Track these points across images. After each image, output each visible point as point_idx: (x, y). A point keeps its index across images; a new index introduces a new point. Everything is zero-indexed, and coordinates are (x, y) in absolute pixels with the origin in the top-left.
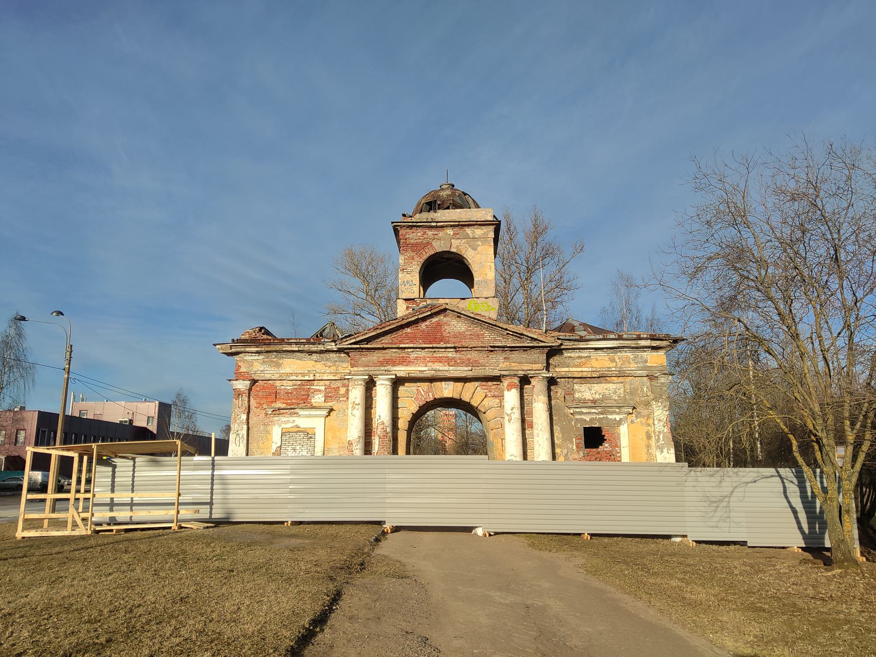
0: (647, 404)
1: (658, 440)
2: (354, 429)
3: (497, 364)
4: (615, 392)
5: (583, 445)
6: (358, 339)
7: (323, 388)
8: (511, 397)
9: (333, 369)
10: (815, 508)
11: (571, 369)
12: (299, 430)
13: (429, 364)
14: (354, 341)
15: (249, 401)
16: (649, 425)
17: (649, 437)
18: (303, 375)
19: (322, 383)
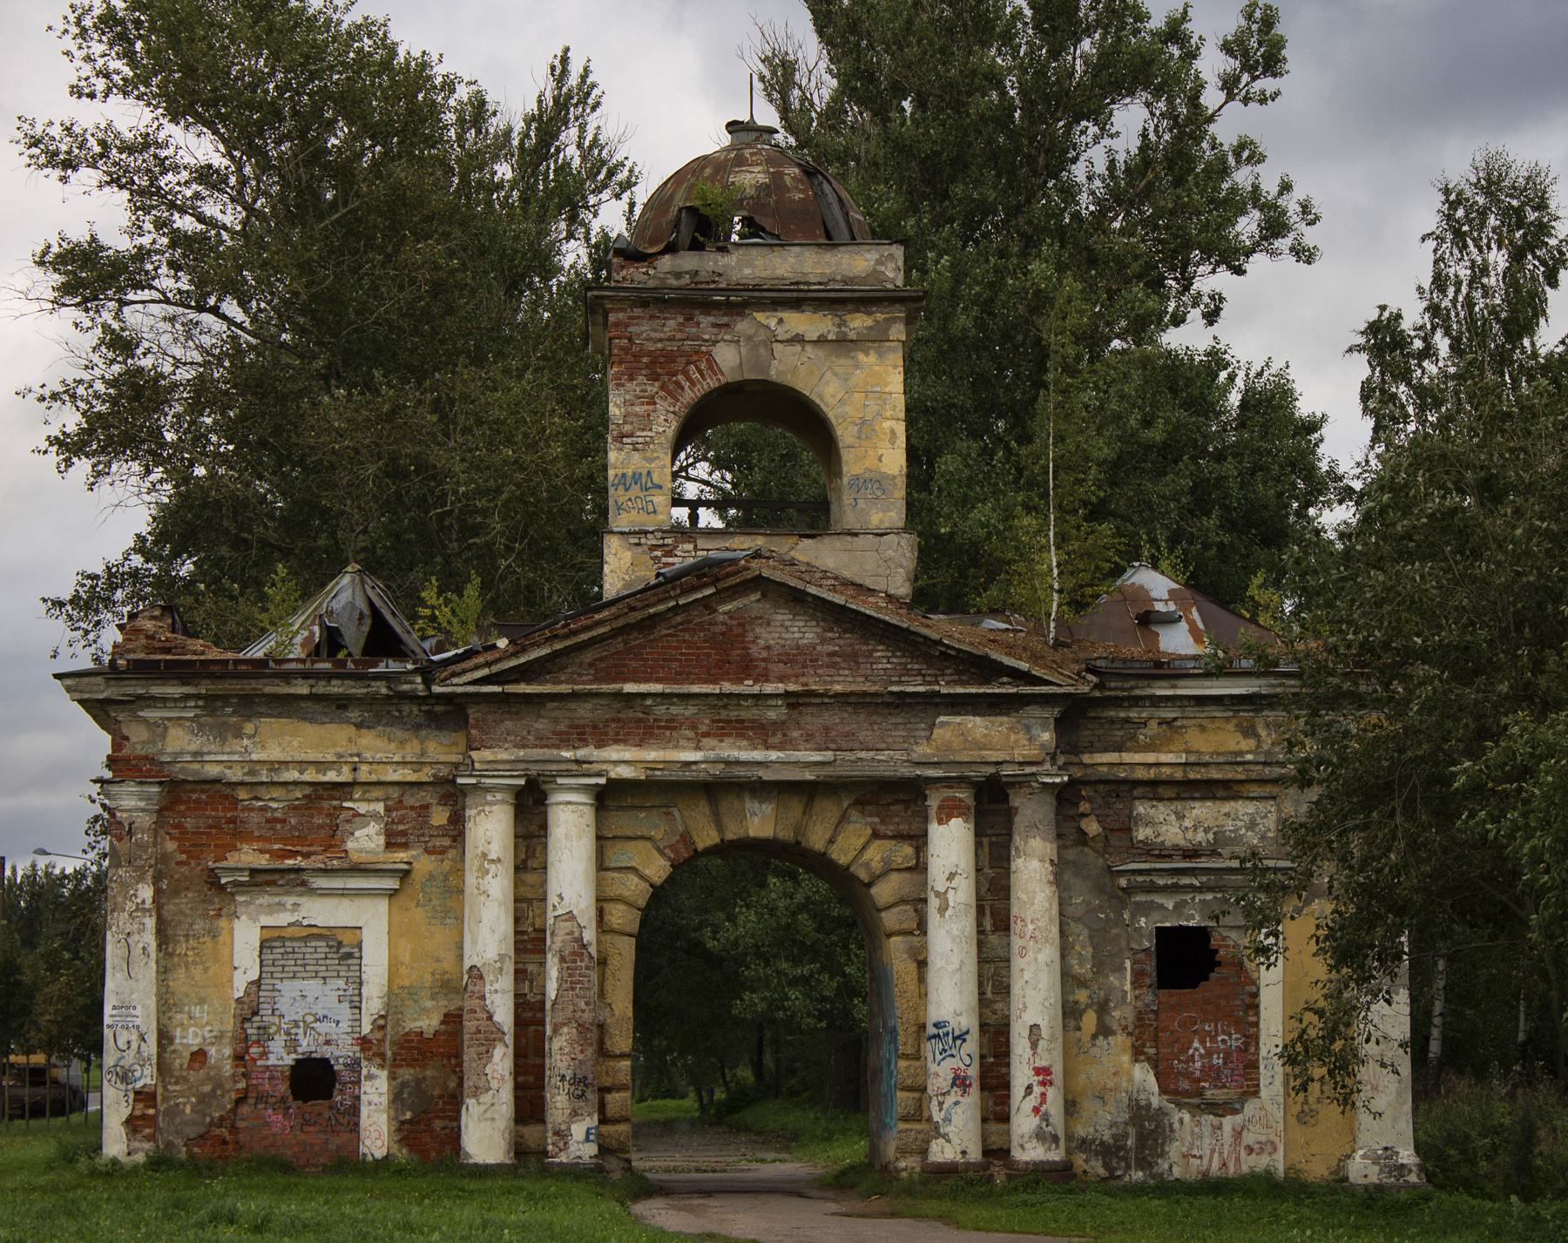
2: (489, 933)
3: (888, 753)
4: (1252, 825)
5: (1151, 979)
6: (495, 669)
7: (380, 807)
8: (951, 844)
9: (411, 750)
10: (1061, 872)
11: (1128, 757)
12: (315, 934)
18: (321, 766)
19: (377, 792)
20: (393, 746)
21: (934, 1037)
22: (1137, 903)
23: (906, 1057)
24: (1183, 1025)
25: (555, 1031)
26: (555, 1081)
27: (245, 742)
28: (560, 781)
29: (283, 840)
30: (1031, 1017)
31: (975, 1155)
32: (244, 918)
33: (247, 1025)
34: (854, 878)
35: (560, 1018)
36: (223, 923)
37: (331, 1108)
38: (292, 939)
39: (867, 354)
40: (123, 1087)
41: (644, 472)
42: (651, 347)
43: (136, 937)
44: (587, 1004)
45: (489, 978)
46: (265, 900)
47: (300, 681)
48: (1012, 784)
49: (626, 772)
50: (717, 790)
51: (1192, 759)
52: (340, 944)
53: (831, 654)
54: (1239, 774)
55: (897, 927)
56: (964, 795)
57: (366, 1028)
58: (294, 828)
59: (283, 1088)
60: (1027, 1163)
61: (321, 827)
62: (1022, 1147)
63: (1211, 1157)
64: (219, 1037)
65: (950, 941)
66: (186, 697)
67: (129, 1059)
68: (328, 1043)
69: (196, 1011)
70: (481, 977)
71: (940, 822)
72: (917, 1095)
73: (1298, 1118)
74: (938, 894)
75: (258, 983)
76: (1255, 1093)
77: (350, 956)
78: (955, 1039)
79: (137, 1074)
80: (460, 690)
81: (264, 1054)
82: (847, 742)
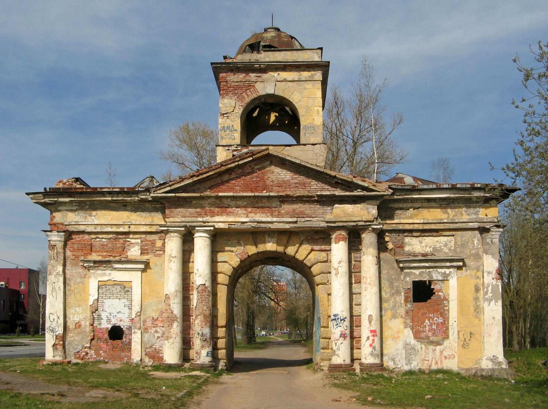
0: (478, 257)
1: (486, 293)
2: (172, 283)
4: (446, 245)
5: (411, 299)
6: (173, 187)
7: (139, 241)
8: (339, 250)
12: (116, 283)
13: (250, 215)
14: (169, 189)
15: (65, 253)
16: (478, 278)
17: (477, 290)
20: (142, 219)
21: (334, 320)
22: (406, 273)
23: (324, 327)
24: (422, 315)
25: (196, 317)
26: (196, 335)
27: (93, 218)
28: (197, 228)
29: (107, 252)
30: (369, 312)
31: (348, 361)
32: (93, 278)
33: (94, 314)
34: (305, 265)
35: (198, 313)
36: (86, 279)
37: (122, 343)
38: (109, 285)
39: (309, 85)
40: (52, 334)
41: (231, 126)
42: (233, 84)
43: (56, 284)
44: (207, 308)
45: (172, 298)
46: (99, 272)
47: (108, 195)
48: (361, 229)
49: (222, 226)
50: (256, 235)
51: (425, 222)
52: (125, 287)
53: (296, 183)
54: (441, 227)
55: (320, 282)
56: (343, 233)
57: (133, 316)
58: (110, 247)
59: (106, 336)
60: (367, 364)
61: (119, 247)
62: (366, 358)
63: (432, 361)
64: (85, 319)
65: (338, 285)
66: (71, 202)
67: (54, 325)
68: (121, 321)
69: (78, 309)
70: (169, 298)
71: (336, 243)
72: (328, 340)
73: (463, 347)
74: (335, 269)
75: (97, 300)
76: (447, 337)
77: (128, 291)
78: (341, 320)
79: (57, 330)
80: (160, 195)
81: (100, 324)
82: (301, 215)
